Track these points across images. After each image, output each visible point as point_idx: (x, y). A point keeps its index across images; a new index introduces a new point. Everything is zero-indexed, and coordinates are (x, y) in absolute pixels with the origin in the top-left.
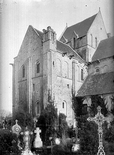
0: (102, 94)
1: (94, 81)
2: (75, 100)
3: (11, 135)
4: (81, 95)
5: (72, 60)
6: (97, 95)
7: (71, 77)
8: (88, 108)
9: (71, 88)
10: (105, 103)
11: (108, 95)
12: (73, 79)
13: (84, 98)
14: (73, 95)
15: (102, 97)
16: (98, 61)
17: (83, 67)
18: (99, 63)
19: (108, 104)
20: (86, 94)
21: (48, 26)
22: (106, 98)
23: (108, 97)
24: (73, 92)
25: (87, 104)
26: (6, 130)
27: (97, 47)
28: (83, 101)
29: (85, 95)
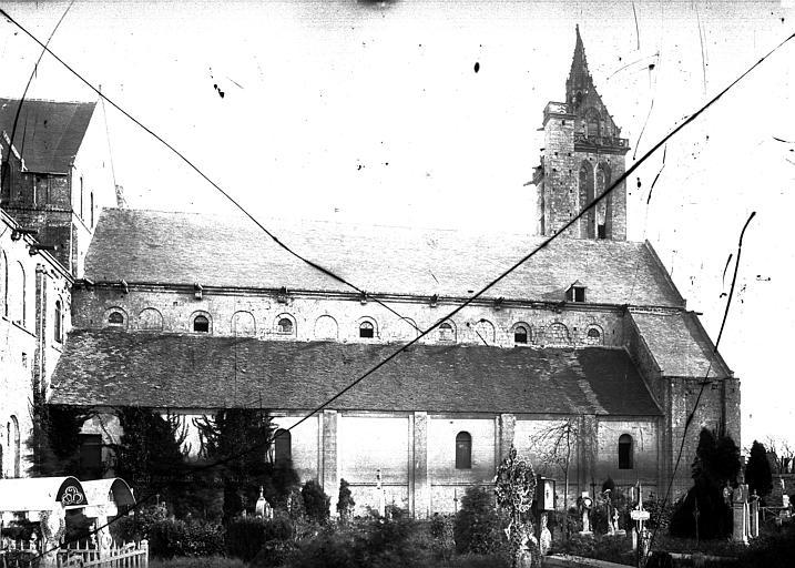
0: (168, 408)
1: (109, 352)
2: (45, 417)
3: (220, 553)
4: (68, 400)
5: (37, 258)
6: (147, 410)
7: (31, 325)
8: (104, 449)
9: (30, 362)
10: (177, 438)
11: (188, 411)
12: (39, 333)
13: (90, 412)
14: (38, 396)
15: (165, 417)
16: (123, 286)
17: (60, 292)
18: (126, 293)
19: (187, 441)
20: (99, 398)
21: (465, 430)
22: (181, 421)
23: (189, 418)
24: (36, 383)
25: (101, 435)
26: (470, 522)
27: (95, 226)
28: (81, 423)
29: (94, 402)
